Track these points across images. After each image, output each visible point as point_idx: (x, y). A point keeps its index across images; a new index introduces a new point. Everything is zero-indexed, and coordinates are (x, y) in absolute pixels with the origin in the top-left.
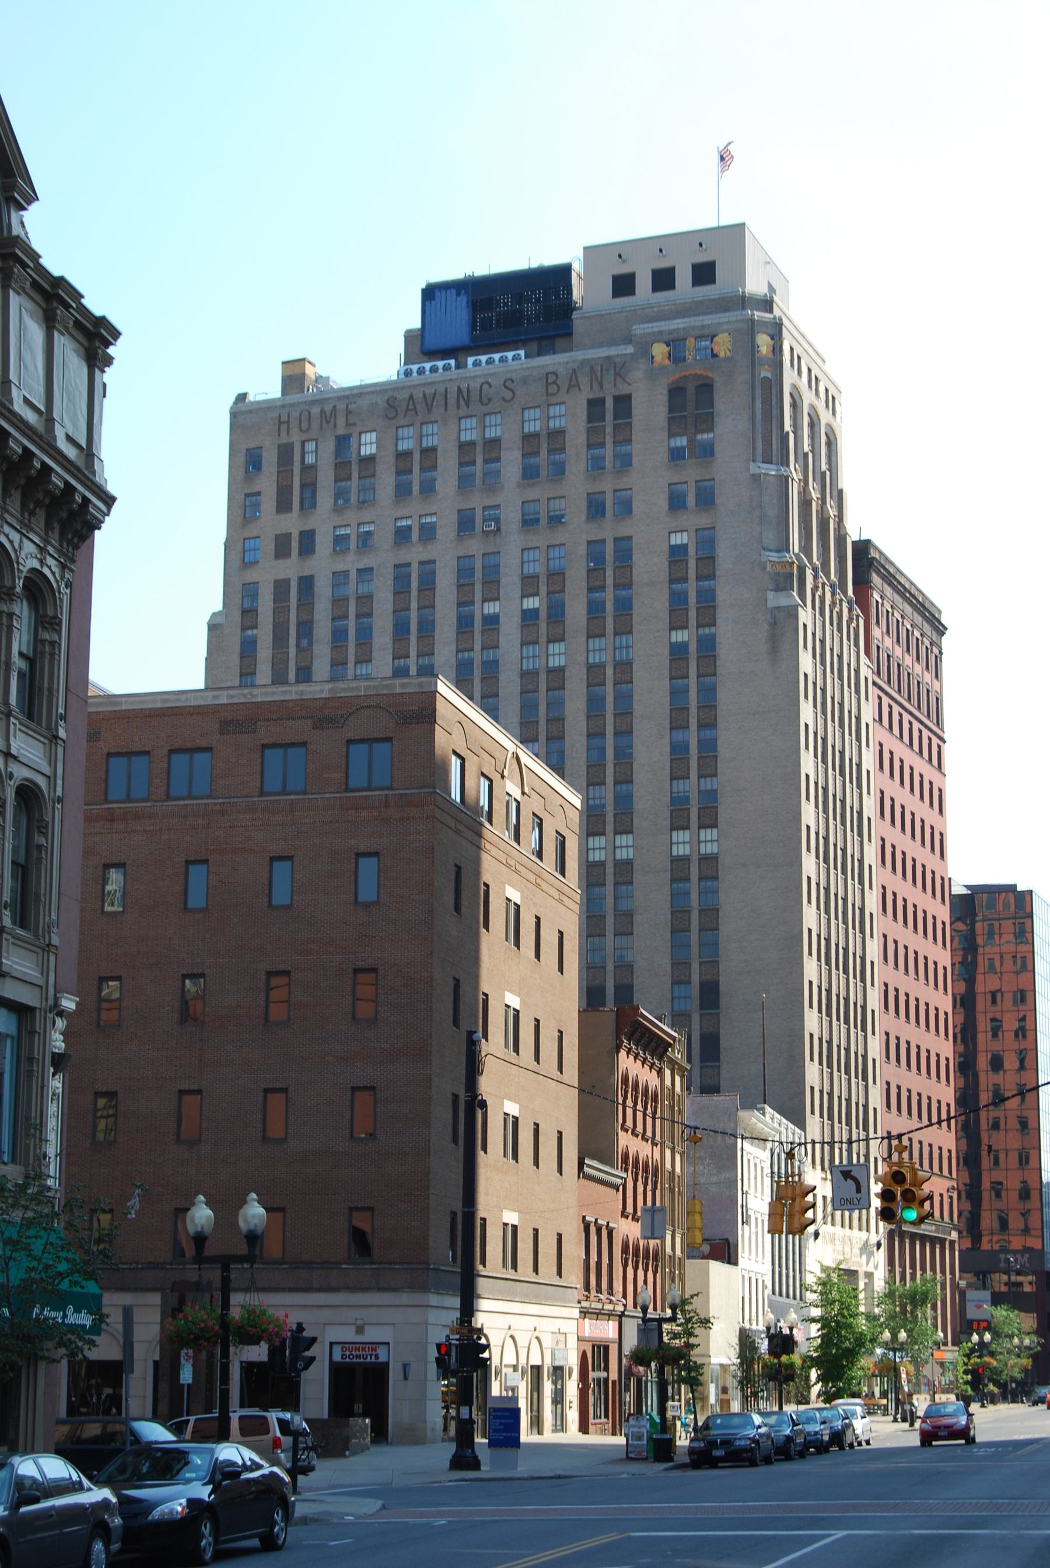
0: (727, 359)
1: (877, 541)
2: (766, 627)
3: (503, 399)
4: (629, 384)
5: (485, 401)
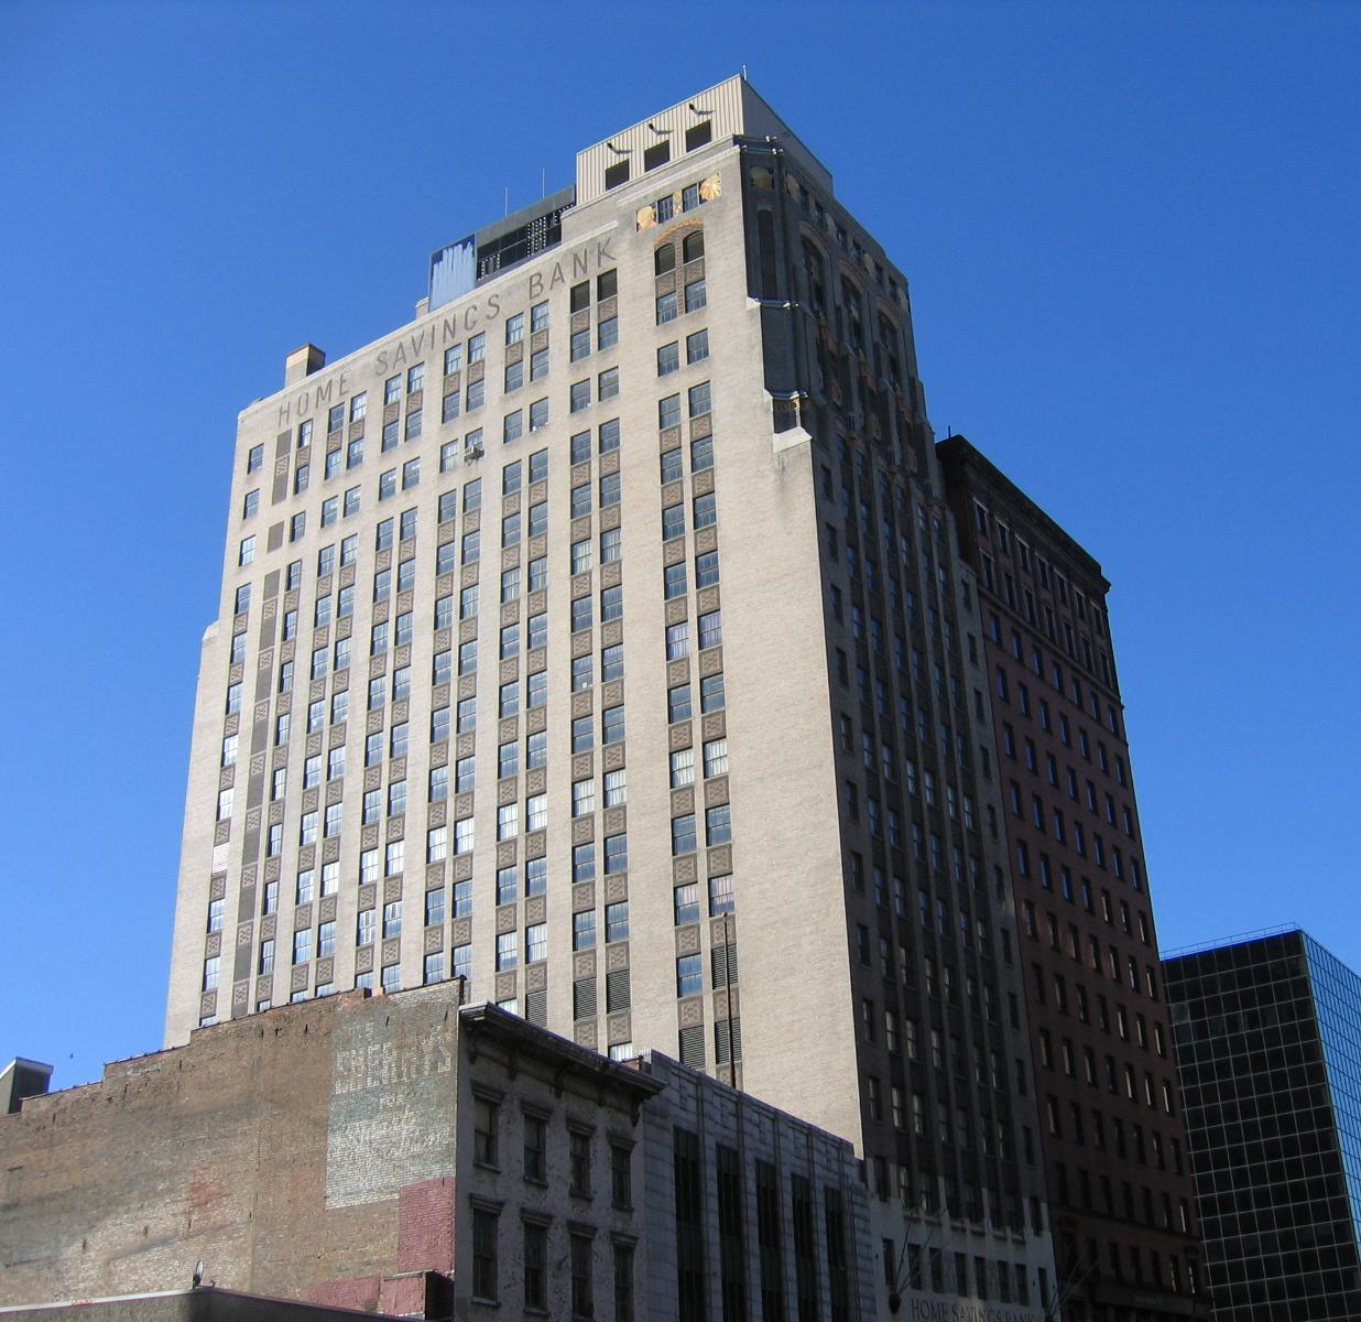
0: (718, 200)
1: (1306, 930)
2: (773, 477)
3: (488, 317)
4: (614, 259)
5: (469, 325)
